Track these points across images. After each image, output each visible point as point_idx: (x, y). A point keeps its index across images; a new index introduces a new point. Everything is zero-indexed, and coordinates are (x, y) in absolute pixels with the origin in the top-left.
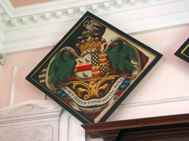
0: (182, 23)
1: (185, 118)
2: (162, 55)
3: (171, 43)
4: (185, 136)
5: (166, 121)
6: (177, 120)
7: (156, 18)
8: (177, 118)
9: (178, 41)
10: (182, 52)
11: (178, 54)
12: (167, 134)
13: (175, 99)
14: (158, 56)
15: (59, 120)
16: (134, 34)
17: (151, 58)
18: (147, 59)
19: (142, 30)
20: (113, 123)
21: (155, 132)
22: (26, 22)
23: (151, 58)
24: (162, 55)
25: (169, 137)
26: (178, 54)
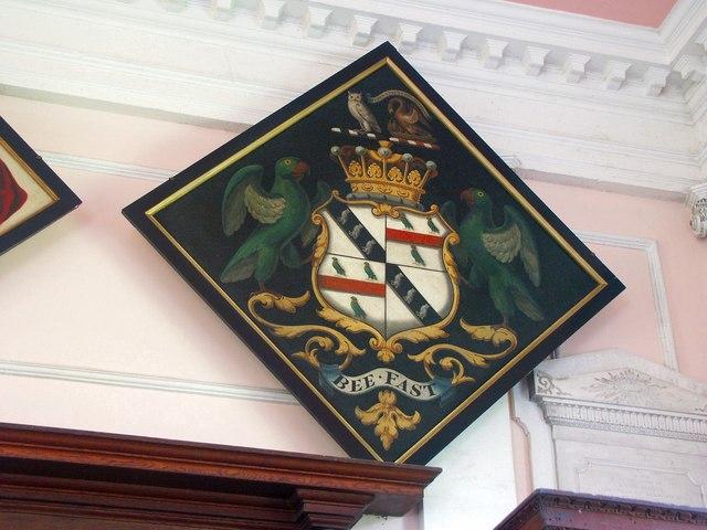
0: (175, 110)
1: (140, 452)
2: (79, 202)
3: (120, 166)
4: (73, 512)
5: (21, 447)
6: (61, 450)
7: (190, 78)
8: (34, 437)
9: (146, 169)
10: (150, 212)
11: (135, 212)
12: (12, 495)
13: (79, 374)
14: (65, 201)
15: (554, 441)
16: (534, 174)
17: (37, 198)
18: (20, 197)
19: (31, 86)
20: (147, 443)
21: (109, 491)
22: (693, 72)
23: (37, 198)
24: (79, 202)
25: (14, 507)
26: (135, 212)
